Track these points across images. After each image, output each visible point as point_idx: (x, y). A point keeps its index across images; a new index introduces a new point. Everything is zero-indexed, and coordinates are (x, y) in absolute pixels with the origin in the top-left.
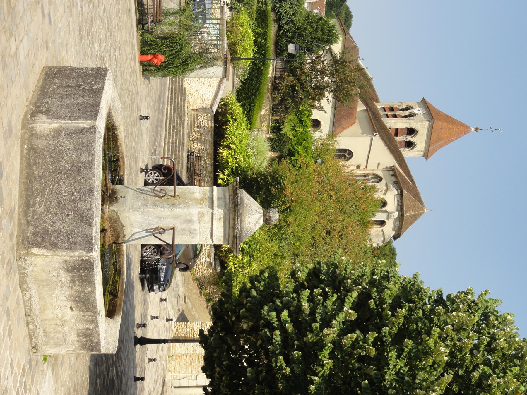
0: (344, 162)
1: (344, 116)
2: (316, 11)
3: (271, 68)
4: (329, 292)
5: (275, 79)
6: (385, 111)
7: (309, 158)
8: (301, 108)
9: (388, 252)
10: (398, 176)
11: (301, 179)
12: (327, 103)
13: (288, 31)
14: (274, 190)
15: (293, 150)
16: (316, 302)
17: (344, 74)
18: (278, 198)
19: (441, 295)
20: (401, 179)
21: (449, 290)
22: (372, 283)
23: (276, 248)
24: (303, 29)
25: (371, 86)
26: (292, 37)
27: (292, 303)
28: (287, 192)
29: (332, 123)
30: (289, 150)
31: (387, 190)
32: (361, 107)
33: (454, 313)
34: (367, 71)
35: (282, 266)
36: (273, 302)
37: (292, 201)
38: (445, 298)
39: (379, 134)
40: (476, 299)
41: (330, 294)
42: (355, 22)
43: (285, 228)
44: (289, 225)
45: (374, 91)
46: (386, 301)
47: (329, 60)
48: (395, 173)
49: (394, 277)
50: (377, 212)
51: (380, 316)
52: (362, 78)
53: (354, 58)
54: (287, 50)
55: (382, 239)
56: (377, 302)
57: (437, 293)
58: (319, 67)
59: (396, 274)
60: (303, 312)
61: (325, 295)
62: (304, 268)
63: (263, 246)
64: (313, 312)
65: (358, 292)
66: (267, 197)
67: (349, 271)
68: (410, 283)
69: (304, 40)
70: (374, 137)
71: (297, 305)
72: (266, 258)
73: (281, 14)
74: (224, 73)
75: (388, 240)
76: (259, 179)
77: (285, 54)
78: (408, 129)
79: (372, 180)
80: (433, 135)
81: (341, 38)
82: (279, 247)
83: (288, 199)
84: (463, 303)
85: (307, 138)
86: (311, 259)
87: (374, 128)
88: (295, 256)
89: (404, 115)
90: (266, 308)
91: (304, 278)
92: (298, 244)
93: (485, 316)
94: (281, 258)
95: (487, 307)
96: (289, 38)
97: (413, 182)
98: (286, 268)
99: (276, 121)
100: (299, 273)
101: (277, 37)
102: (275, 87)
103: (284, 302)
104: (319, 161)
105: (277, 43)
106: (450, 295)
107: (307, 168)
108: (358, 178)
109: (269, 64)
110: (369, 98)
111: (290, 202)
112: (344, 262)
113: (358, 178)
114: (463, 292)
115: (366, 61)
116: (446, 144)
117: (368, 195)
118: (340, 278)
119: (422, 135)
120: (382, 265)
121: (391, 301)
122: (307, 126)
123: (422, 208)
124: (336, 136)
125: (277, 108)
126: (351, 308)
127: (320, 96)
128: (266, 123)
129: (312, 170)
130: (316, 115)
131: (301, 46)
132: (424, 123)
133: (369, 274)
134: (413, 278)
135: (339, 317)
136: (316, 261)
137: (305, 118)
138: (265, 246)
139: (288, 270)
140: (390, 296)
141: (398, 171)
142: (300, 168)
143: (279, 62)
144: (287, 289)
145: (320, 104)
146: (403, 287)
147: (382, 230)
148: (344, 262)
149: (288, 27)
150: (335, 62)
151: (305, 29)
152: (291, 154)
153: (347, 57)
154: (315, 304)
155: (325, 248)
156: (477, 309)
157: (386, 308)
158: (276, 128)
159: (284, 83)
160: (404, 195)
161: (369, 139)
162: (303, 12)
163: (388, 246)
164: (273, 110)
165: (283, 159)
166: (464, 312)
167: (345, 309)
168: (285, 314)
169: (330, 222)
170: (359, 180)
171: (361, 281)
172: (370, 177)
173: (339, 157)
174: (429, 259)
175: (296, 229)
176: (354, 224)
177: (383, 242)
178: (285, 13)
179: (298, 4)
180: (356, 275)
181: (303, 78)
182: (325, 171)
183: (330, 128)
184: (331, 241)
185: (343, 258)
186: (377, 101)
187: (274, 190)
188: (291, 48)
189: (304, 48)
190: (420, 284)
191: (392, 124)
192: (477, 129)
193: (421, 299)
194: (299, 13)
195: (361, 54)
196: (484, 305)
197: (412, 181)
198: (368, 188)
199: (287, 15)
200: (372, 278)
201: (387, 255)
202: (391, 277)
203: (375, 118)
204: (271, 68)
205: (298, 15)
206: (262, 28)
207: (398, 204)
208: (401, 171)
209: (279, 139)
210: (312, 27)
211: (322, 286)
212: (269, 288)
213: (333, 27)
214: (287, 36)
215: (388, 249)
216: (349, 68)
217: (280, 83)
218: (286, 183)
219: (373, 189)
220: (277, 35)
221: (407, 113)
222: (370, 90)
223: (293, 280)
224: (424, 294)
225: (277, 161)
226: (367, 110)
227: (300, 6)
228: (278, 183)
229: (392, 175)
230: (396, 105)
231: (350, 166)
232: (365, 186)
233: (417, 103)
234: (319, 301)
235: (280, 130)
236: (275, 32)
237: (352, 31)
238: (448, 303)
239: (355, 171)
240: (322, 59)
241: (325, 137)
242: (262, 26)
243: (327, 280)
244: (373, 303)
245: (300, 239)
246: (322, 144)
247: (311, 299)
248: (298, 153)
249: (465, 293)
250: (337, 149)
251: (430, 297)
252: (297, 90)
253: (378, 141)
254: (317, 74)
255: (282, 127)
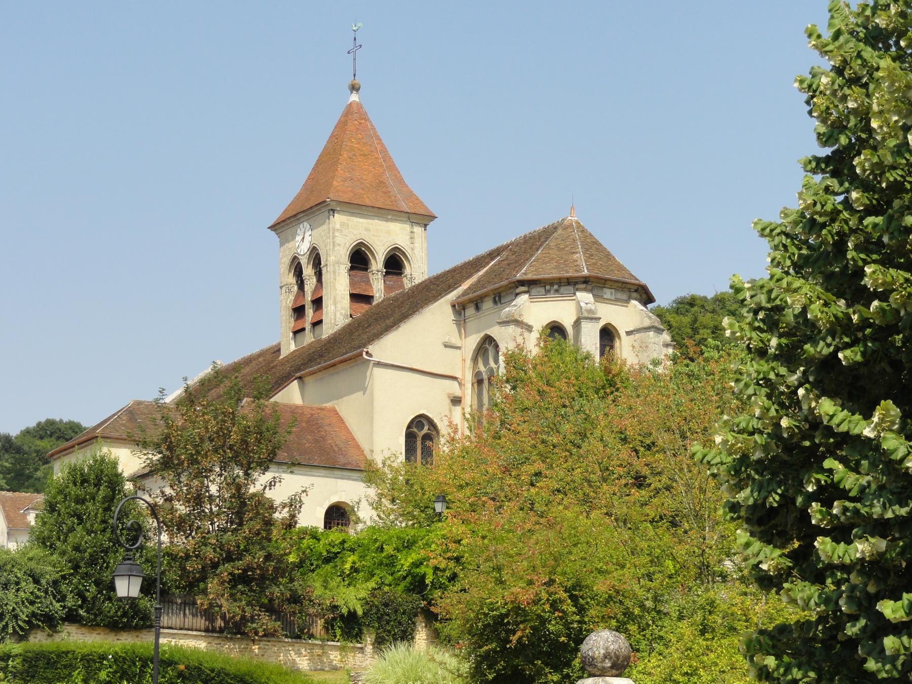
0: (442, 440)
1: (316, 441)
2: (31, 518)
3: (182, 642)
4: (818, 481)
5: (214, 630)
6: (303, 330)
7: (432, 535)
8: (292, 558)
9: (687, 320)
10: (479, 293)
11: (488, 559)
12: (279, 487)
13: (81, 595)
14: (519, 634)
15: (409, 579)
16: (848, 518)
17: (202, 440)
18: (544, 621)
19: (818, 160)
20: (488, 284)
21: (805, 139)
22: (788, 356)
23: (686, 628)
24: (78, 555)
25: (235, 368)
26: (97, 583)
27: (853, 588)
28: (525, 596)
29: (337, 472)
30: (408, 590)
31: (518, 323)
32: (292, 395)
33: (874, 124)
34: (193, 381)
35: (735, 609)
36: (852, 643)
37: (551, 582)
38: (827, 151)
39: (365, 345)
40: (827, 64)
41: (822, 478)
42: (63, 414)
43: (628, 603)
44: (617, 592)
45: (248, 361)
46: (840, 315)
47: (161, 483)
48: (471, 301)
49: (770, 291)
50: (577, 350)
51: (884, 332)
52: (213, 393)
53: (158, 416)
54: (132, 601)
55: (651, 333)
56: (846, 340)
57: (814, 171)
58: (182, 509)
59: (762, 287)
60: (881, 555)
61: (829, 493)
62: (749, 551)
63: (678, 663)
64: (880, 527)
65: (818, 397)
66: (540, 655)
67: (755, 423)
68: (785, 246)
69: (106, 551)
70: (375, 359)
71: (861, 573)
72: (712, 656)
73: (34, 614)
74: (341, 366)
75: (654, 317)
76: (490, 677)
77: (146, 603)
78: (352, 268)
79: (492, 364)
80: (368, 202)
81: (105, 450)
82: (681, 618)
83: (544, 596)
84: (844, 98)
85: (376, 540)
86: (712, 528)
87: (350, 359)
88: (705, 572)
89: (314, 280)
90: (871, 665)
91: (778, 552)
92: (669, 564)
93: (876, 38)
94: (710, 613)
95: (851, 33)
96: (100, 592)
97: (497, 252)
98: (738, 600)
99: (329, 626)
100: (764, 567)
101: (98, 625)
102: (236, 629)
103: (853, 610)
104: (439, 507)
105: (114, 626)
106: (819, 134)
107: (459, 542)
108: (486, 400)
109: (170, 647)
110: (267, 372)
111: (552, 589)
112: (730, 438)
113: (486, 400)
114: (808, 103)
115: (168, 383)
116: (392, 167)
117: (531, 373)
118: (776, 451)
119: (367, 230)
120: (736, 328)
121: (842, 302)
122: (344, 542)
123: (565, 228)
124: (370, 463)
125: (291, 623)
126: (867, 416)
127: (263, 506)
128: (335, 656)
129: (463, 528)
130: (312, 517)
131: (124, 559)
132: (338, 226)
133: (765, 367)
134: (773, 238)
135: (896, 450)
136: (725, 514)
137: (321, 547)
138: (680, 659)
139: (745, 594)
140: (826, 304)
141: (465, 293)
142: (457, 559)
143: (165, 620)
144: (812, 602)
145: (284, 506)
146: (798, 267)
147: (629, 333)
148: (730, 438)
149: (70, 596)
150: (166, 464)
151: (77, 548)
152: (418, 585)
153: (155, 435)
154: (857, 520)
155: (682, 489)
156: (859, 62)
157: (861, 316)
158: (349, 626)
159: (226, 605)
160: (530, 276)
161: (378, 371)
162: (30, 555)
163: (669, 317)
164: (299, 637)
165: (432, 609)
166: (868, 95)
167: (868, 432)
168: (889, 609)
169: (606, 474)
170: (490, 399)
171: (783, 388)
172: (482, 368)
173: (427, 453)
174: (713, 198)
175: (628, 573)
176: (613, 410)
177: (659, 331)
178: (32, 603)
179: (8, 567)
180: (767, 403)
181: (210, 553)
182: (468, 491)
183: (348, 479)
184: (660, 473)
185: (718, 439)
186: (277, 350)
187: (519, 634)
188: (127, 588)
189: (128, 550)
190: (790, 219)
191: (338, 312)
192: (354, 88)
193: (834, 215)
194: (32, 564)
195: (148, 396)
196: (847, 42)
197: (491, 255)
198: (514, 373)
199: (37, 597)
200: (776, 358)
201: (695, 320)
202: (769, 300)
203: (321, 356)
204: (182, 642)
205: (39, 568)
206: (71, 667)
207: (557, 291)
208: (465, 286)
209: (379, 619)
210: (72, 530)
211: (800, 500)
212: (811, 654)
213: (73, 471)
214: (95, 598)
215: (678, 318)
216: (183, 428)
217: (223, 617)
218: (500, 599)
219: (515, 361)
220: (92, 624)
221: (308, 271)
222: (245, 371)
223: (786, 585)
224: (818, 207)
225: (438, 625)
226: (300, 378)
227: (14, 563)
228: (502, 623)
229: (477, 308)
230: (289, 300)
231: (453, 424)
232: (507, 381)
233: (282, 244)
234: (845, 509)
235: (352, 615)
236: (84, 630)
237: (89, 418)
238: (843, 140)
239: (468, 410)
240: (160, 501)
241: (372, 492)
242: (65, 667)
243: (781, 489)
244: (848, 352)
245: (656, 561)
246: (393, 501)
247: (841, 533)
248: (417, 564)
249: (813, 97)
250: (408, 458)
251: (827, 190)
252: (245, 571)
253: (384, 349)
254: (201, 516)
255: (345, 611)
